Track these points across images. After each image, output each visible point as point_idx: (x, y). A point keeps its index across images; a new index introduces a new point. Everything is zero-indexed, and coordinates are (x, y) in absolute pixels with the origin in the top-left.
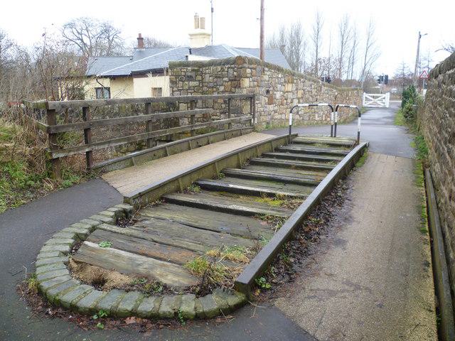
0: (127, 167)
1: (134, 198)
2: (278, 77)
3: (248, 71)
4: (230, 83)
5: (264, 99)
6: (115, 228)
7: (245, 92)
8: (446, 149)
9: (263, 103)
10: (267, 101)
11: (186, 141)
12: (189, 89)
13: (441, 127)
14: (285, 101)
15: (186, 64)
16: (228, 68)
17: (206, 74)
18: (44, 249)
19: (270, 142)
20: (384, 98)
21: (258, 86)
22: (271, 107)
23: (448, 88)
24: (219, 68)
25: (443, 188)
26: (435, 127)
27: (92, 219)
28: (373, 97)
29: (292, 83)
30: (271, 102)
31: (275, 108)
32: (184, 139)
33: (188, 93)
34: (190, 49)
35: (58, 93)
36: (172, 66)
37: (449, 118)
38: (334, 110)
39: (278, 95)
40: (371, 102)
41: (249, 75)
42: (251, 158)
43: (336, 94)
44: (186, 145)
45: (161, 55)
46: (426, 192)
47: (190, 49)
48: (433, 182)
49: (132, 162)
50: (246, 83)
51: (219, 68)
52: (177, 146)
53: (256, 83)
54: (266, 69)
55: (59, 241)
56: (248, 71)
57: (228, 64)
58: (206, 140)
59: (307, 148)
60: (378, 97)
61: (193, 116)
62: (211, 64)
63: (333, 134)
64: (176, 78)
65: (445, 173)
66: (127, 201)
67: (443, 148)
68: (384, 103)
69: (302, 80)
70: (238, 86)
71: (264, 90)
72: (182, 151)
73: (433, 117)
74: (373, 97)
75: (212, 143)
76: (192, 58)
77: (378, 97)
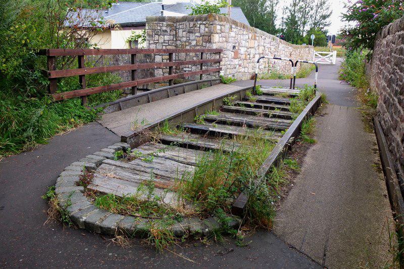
0: (116, 111)
1: (131, 137)
2: (243, 34)
3: (218, 27)
4: (201, 38)
5: (231, 54)
6: (118, 163)
7: (215, 46)
8: (396, 100)
9: (230, 57)
10: (233, 56)
11: (181, 86)
12: (164, 43)
13: (390, 82)
14: (248, 56)
15: (162, 19)
16: (200, 24)
17: (179, 29)
18: (63, 174)
19: (238, 92)
20: (332, 56)
21: (226, 42)
22: (236, 62)
23: (399, 47)
24: (192, 24)
25: (394, 133)
26: (383, 81)
27: (97, 155)
28: (321, 54)
29: (255, 39)
30: (236, 56)
31: (240, 62)
32: (158, 89)
33: (163, 46)
34: (163, 6)
35: (325, 51)
36: (149, 20)
37: (400, 73)
38: (294, 65)
39: (243, 50)
40: (320, 59)
41: (219, 31)
42: (221, 104)
43: (291, 50)
44: (165, 93)
45: (136, 9)
46: (377, 138)
47: (163, 6)
48: (383, 129)
49: (211, 84)
50: (216, 38)
51: (192, 24)
52: (158, 94)
53: (224, 39)
54: (233, 26)
55: (70, 173)
56: (218, 27)
57: (200, 20)
58: (181, 89)
59: (270, 98)
60: (327, 55)
61: (81, 77)
62: (184, 19)
63: (292, 86)
64: (153, 32)
65: (396, 121)
66: (124, 139)
67: (393, 99)
68: (331, 60)
69: (263, 37)
70: (209, 41)
71: (230, 46)
72: (162, 98)
73: (380, 72)
74: (321, 54)
75: (187, 92)
76: (167, 14)
77: (327, 55)
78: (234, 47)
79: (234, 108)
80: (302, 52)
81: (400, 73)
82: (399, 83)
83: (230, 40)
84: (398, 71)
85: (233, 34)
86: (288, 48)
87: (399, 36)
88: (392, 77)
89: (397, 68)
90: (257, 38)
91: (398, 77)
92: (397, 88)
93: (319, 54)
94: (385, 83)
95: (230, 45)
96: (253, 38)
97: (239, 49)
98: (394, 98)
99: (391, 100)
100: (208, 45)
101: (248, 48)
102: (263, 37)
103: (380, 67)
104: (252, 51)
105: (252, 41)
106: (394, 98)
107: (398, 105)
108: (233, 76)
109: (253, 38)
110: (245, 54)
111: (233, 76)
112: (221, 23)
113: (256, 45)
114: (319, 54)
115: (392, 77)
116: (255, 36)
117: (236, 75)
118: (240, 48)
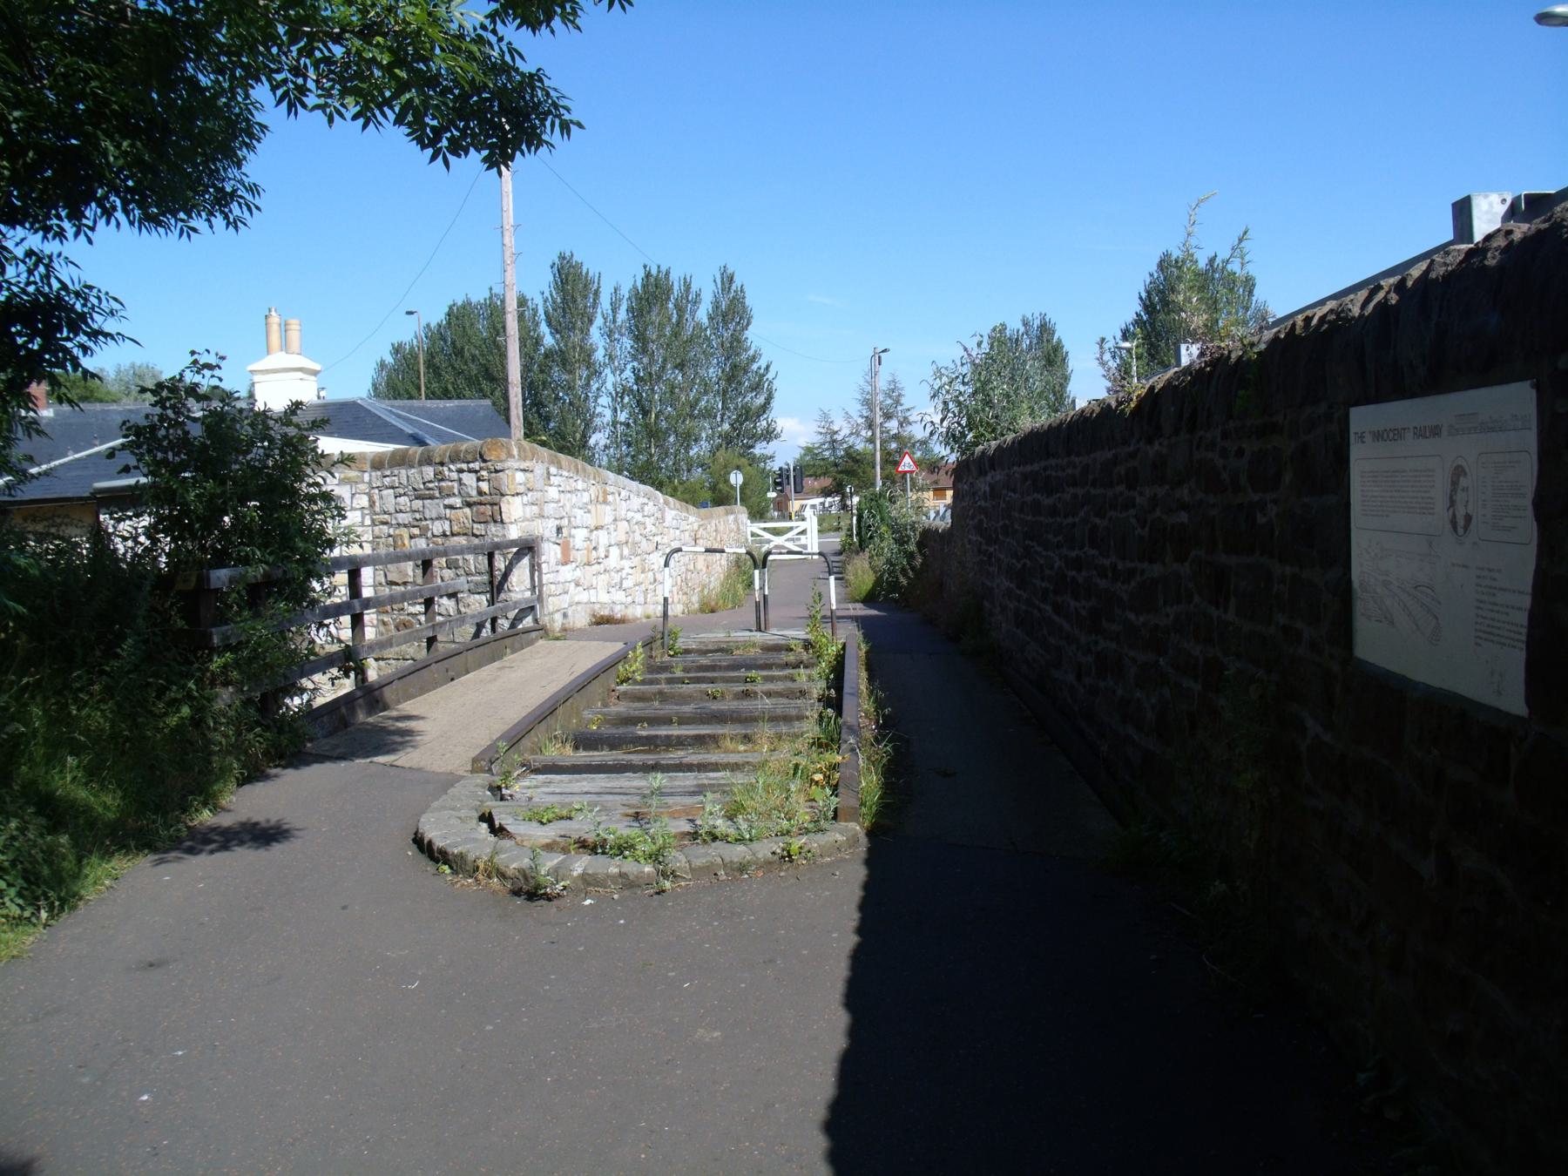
7: (514, 533)
10: (559, 556)
20: (803, 532)
23: (1029, 499)
29: (605, 502)
31: (578, 573)
37: (1044, 553)
50: (513, 509)
67: (1040, 610)
70: (497, 519)
78: (559, 530)
79: (753, 673)
80: (721, 528)
81: (1044, 553)
82: (1047, 572)
83: (549, 509)
84: (1039, 549)
85: (553, 493)
86: (686, 519)
87: (1025, 477)
88: (1025, 565)
89: (1035, 544)
90: (610, 498)
91: (1042, 562)
92: (1043, 585)
93: (764, 529)
94: (1007, 584)
95: (550, 526)
96: (601, 499)
97: (570, 536)
98: (1042, 606)
99: (1036, 611)
100: (493, 528)
101: (592, 531)
102: (624, 493)
103: (984, 547)
104: (602, 538)
105: (599, 506)
106: (1042, 606)
107: (1055, 617)
108: (565, 615)
109: (601, 499)
110: (587, 549)
111: (565, 615)
112: (524, 465)
113: (608, 519)
114: (764, 529)
115: (1025, 565)
116: (606, 493)
117: (570, 613)
118: (573, 530)
